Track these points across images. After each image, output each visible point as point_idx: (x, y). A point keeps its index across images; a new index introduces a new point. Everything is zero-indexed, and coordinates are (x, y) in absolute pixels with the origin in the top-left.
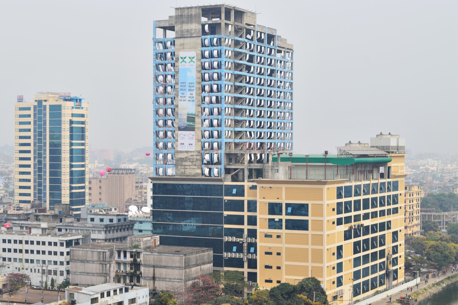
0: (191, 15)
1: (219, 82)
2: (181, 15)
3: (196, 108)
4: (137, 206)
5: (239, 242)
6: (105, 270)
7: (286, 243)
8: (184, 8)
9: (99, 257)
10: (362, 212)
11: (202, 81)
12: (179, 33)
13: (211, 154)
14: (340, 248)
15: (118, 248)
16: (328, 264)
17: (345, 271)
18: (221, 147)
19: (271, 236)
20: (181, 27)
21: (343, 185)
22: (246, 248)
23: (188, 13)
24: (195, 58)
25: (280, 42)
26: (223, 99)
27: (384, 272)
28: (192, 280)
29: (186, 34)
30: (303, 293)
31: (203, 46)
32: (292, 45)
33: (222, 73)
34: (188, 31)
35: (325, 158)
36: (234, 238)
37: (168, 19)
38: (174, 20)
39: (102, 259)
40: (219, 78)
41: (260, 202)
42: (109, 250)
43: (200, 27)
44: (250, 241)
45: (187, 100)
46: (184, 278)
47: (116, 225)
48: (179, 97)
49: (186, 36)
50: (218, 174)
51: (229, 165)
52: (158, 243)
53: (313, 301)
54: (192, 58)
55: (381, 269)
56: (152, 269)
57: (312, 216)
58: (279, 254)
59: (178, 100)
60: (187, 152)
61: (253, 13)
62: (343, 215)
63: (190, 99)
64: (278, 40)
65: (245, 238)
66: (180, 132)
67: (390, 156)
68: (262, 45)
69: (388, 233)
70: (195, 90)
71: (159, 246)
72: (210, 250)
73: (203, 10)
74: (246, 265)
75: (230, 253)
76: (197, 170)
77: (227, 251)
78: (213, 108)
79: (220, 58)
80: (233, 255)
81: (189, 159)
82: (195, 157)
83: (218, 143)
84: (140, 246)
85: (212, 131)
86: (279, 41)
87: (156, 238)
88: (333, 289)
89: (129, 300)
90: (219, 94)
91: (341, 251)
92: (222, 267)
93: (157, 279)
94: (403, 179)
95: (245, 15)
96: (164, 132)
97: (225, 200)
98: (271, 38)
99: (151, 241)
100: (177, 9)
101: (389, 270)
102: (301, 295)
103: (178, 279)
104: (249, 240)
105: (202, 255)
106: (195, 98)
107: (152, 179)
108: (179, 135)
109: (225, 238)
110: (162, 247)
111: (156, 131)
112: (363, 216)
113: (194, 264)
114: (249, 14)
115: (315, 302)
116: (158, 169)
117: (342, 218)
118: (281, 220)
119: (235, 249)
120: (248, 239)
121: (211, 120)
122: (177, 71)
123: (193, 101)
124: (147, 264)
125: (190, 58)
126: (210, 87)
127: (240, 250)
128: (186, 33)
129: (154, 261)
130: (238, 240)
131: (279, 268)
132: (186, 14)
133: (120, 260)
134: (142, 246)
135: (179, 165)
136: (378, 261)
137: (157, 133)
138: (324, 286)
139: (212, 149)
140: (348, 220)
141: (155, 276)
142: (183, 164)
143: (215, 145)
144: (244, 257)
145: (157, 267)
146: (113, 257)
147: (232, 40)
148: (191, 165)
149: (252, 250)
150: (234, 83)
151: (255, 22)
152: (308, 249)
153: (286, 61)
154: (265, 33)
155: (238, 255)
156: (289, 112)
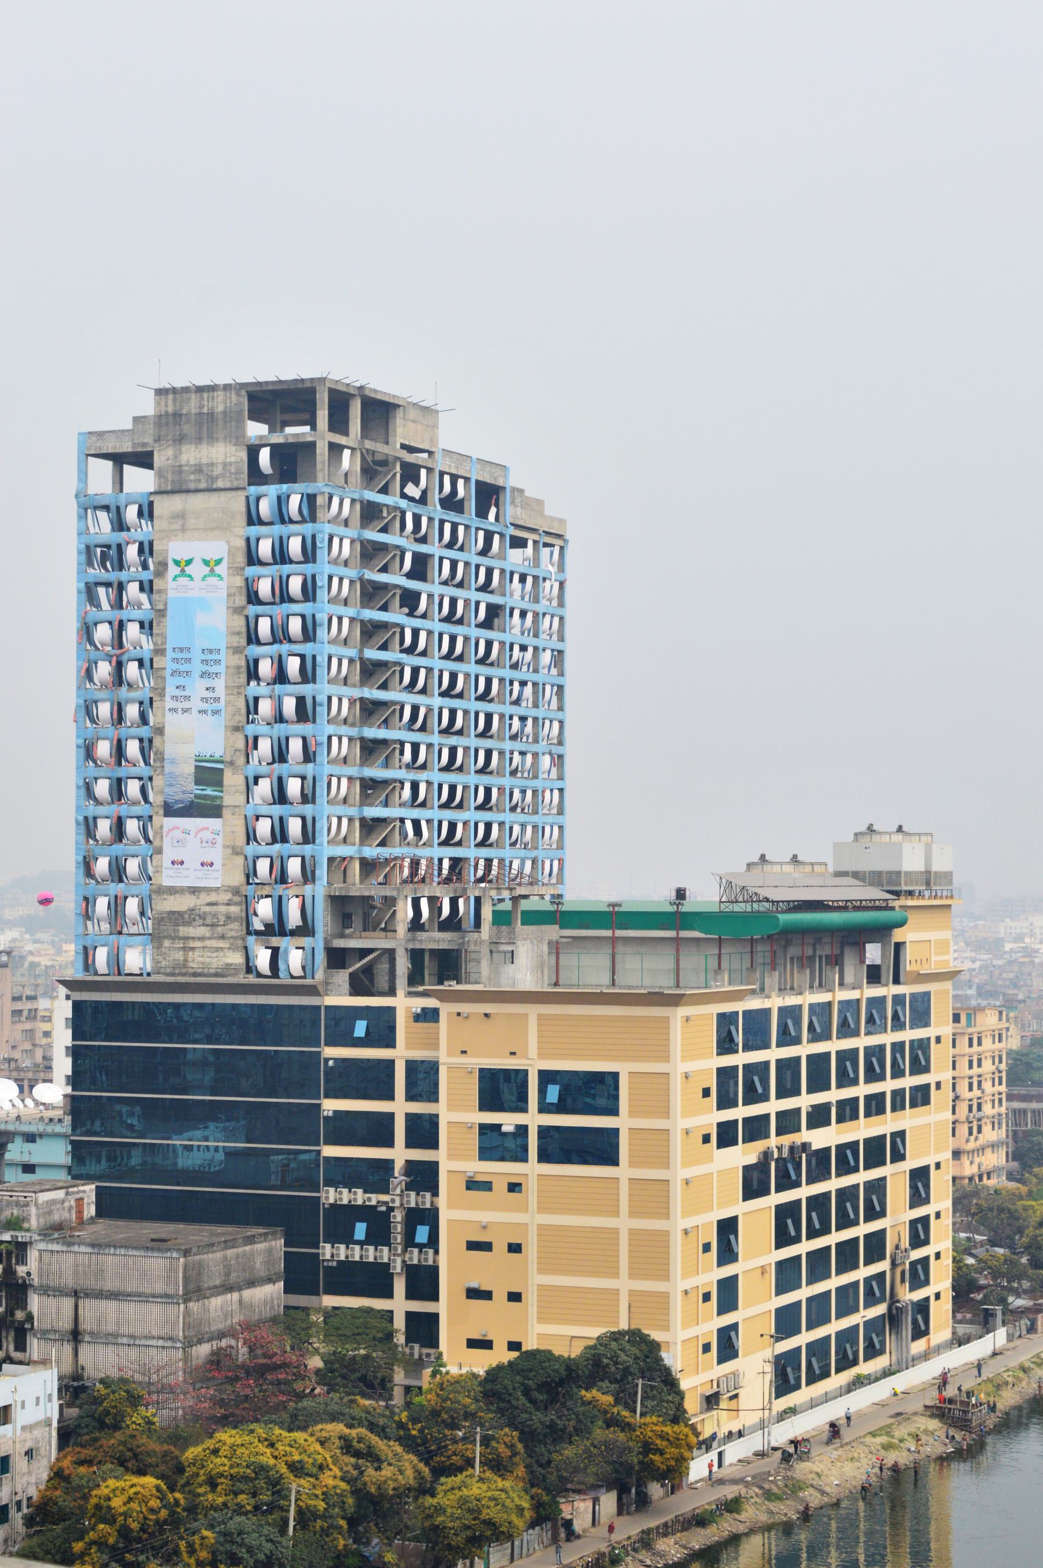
0: (211, 415)
1: (307, 649)
3: (226, 739)
4: (16, 1080)
5: (375, 1207)
7: (541, 1210)
8: (186, 390)
10: (805, 1101)
11: (249, 642)
12: (170, 477)
14: (728, 1227)
16: (688, 1284)
18: (313, 872)
19: (487, 1186)
20: (176, 457)
23: (201, 407)
24: (225, 564)
25: (519, 510)
27: (881, 1309)
28: (210, 1340)
30: (600, 1384)
31: (250, 522)
32: (562, 522)
33: (318, 616)
34: (199, 469)
36: (360, 1191)
37: (129, 425)
38: (151, 431)
43: (243, 455)
44: (413, 1205)
45: (195, 711)
46: (181, 1334)
48: (168, 698)
49: (192, 486)
50: (304, 968)
51: (342, 936)
52: (90, 1211)
53: (635, 1412)
54: (212, 563)
55: (872, 1300)
56: (68, 1303)
57: (632, 1114)
58: (515, 1248)
59: (164, 708)
60: (194, 891)
62: (740, 1113)
63: (205, 706)
64: (513, 502)
67: (901, 907)
68: (457, 520)
70: (223, 676)
74: (399, 1286)
75: (342, 1247)
78: (287, 739)
81: (203, 917)
82: (223, 909)
83: (303, 858)
84: (29, 1221)
85: (281, 818)
86: (516, 506)
87: (84, 1192)
90: (307, 690)
91: (732, 1237)
92: (317, 1294)
93: (87, 1338)
94: (948, 985)
97: (327, 1060)
99: (66, 1204)
100: (160, 392)
101: (898, 1301)
105: (244, 1253)
107: (72, 985)
109: (327, 1192)
112: (808, 1113)
113: (218, 1283)
114: (412, 413)
115: (642, 1415)
116: (91, 953)
118: (522, 1131)
119: (360, 1230)
120: (408, 1196)
121: (280, 779)
123: (216, 712)
124: (51, 1284)
125: (206, 563)
126: (276, 665)
127: (379, 1235)
128: (192, 477)
129: (76, 1273)
130: (374, 1199)
131: (515, 1297)
134: (34, 1223)
135: (165, 937)
136: (862, 1273)
138: (673, 1358)
139: (283, 878)
140: (756, 1128)
142: (181, 934)
143: (294, 867)
145: (87, 1295)
147: (353, 501)
148: (209, 938)
149: (422, 1234)
150: (361, 651)
151: (433, 440)
152: (616, 1231)
153: (541, 575)
154: (467, 480)
155: (371, 1254)
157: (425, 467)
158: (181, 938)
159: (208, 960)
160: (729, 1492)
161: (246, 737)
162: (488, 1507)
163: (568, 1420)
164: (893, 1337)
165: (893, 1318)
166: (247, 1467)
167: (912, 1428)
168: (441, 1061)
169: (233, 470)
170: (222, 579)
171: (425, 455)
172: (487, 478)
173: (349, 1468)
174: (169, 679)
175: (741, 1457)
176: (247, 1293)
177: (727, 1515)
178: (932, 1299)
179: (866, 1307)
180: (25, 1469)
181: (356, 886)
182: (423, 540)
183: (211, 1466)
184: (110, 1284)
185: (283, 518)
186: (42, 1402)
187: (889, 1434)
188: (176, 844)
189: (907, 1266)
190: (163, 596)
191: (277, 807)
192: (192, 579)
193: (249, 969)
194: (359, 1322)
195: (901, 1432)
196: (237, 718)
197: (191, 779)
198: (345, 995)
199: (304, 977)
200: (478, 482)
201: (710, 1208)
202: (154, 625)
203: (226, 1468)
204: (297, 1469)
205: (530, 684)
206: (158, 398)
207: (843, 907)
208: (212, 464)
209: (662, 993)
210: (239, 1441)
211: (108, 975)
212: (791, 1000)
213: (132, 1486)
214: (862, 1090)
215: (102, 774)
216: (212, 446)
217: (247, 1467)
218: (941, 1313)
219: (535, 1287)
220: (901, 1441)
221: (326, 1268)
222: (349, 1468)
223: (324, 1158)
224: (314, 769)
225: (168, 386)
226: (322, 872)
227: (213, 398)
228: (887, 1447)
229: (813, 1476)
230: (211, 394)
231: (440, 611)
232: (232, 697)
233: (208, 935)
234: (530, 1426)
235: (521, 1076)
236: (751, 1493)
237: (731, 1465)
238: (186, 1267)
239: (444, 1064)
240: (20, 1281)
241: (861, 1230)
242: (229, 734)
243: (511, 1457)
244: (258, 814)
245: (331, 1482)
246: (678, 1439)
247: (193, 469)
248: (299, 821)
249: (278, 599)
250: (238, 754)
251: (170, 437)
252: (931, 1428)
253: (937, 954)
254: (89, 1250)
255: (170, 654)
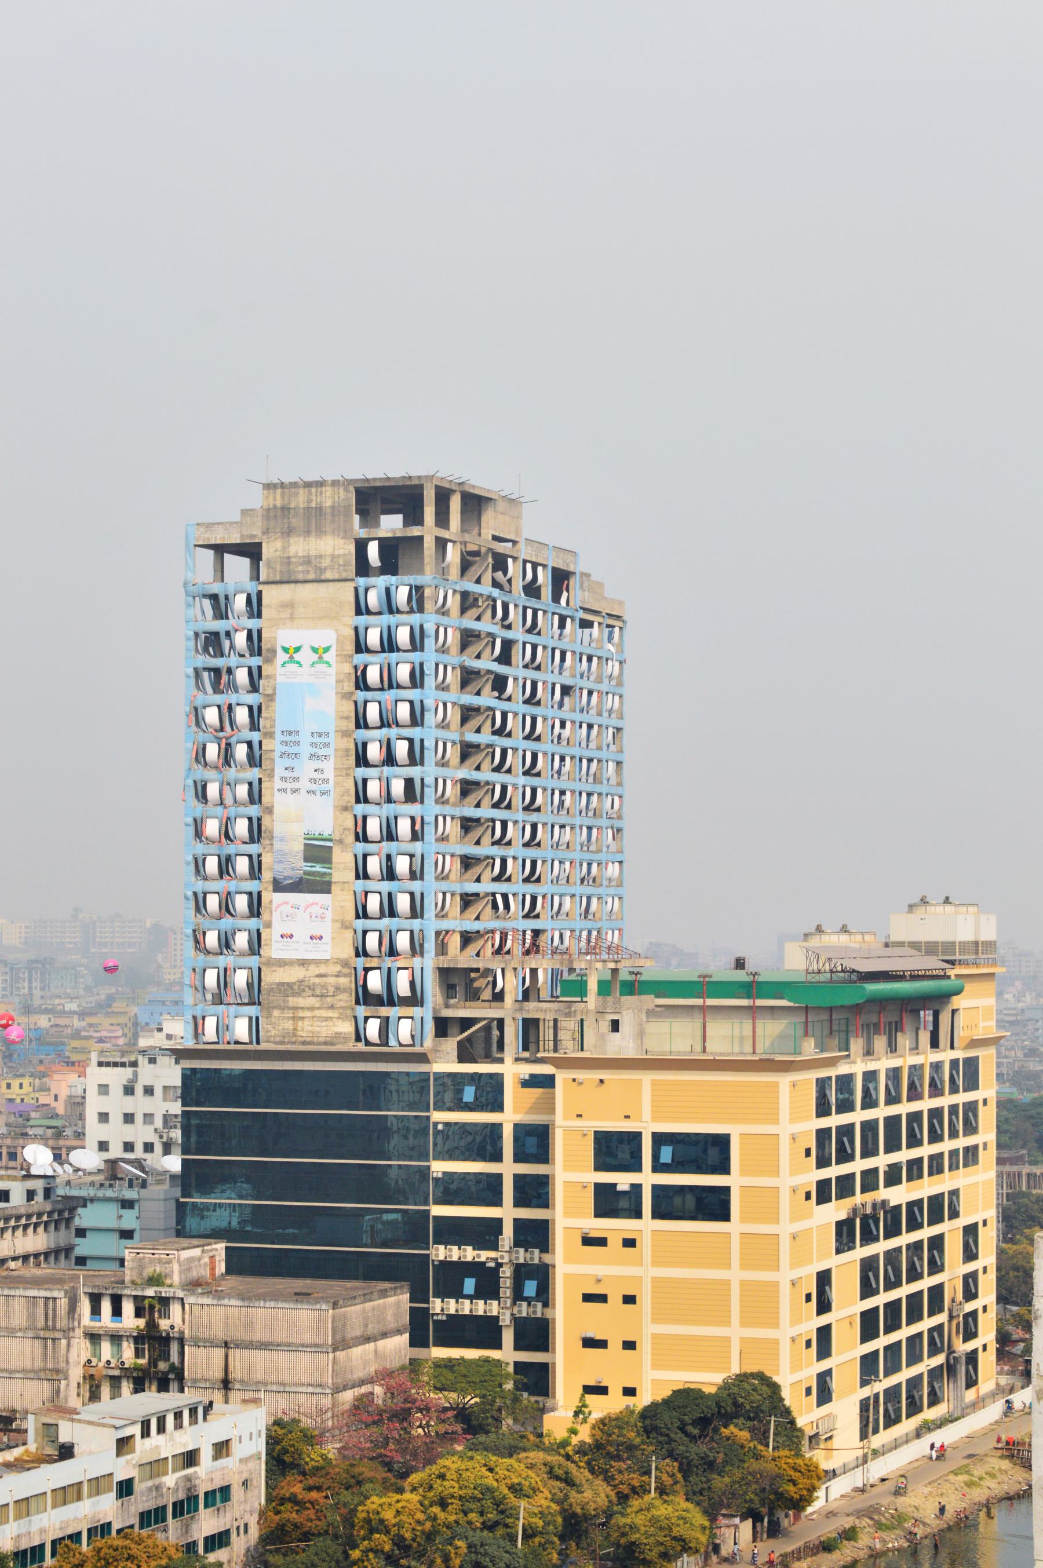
0: (320, 509)
1: (416, 733)
2: (283, 508)
3: (336, 818)
4: (53, 1148)
5: (484, 1263)
6: (54, 1357)
7: (655, 1263)
8: (294, 485)
9: (32, 1317)
10: (882, 1161)
11: (358, 726)
12: (278, 568)
13: (389, 969)
14: (824, 1279)
15: (94, 1287)
16: (794, 1331)
17: (837, 1355)
18: (422, 946)
19: (602, 1242)
20: (284, 548)
21: (832, 1072)
22: (508, 1283)
23: (310, 501)
24: (333, 652)
25: (586, 593)
26: (429, 786)
27: (940, 1359)
28: (353, 1387)
29: (300, 573)
30: (734, 1421)
31: (358, 612)
32: (621, 603)
33: (426, 702)
34: (307, 561)
35: (753, 982)
36: (469, 1249)
37: (237, 518)
38: (260, 524)
39: (41, 1323)
40: (416, 720)
41: (566, 1130)
42: (66, 1292)
43: (352, 548)
44: (521, 1261)
45: (303, 792)
46: (330, 1381)
47: (23, 1211)
48: (277, 779)
49: (301, 577)
50: (413, 1037)
51: (447, 1006)
52: (221, 1268)
53: (767, 1446)
54: (321, 651)
55: (934, 1351)
56: (218, 1353)
57: (744, 1172)
58: (629, 1300)
59: (273, 789)
60: (303, 963)
61: (513, 502)
62: (834, 1171)
63: (313, 787)
64: (581, 587)
65: (507, 1248)
66: (279, 897)
67: (957, 976)
68: (537, 606)
69: (951, 1230)
70: (332, 759)
71: (224, 1279)
72: (402, 1287)
73: (359, 492)
74: (508, 1337)
75: (452, 1301)
76: (339, 1023)
77: (443, 1293)
78: (396, 818)
79: (418, 654)
80: (466, 1307)
81: (312, 988)
82: (332, 980)
83: (412, 932)
84: (171, 1277)
85: (390, 894)
86: (584, 590)
87: (216, 1250)
88: (807, 1413)
89: (215, 1445)
90: (415, 772)
91: (827, 1288)
92: (428, 1346)
93: (237, 1386)
94: (992, 1051)
95: (491, 505)
96: (224, 897)
97: (436, 1124)
98: (561, 578)
99: (202, 1262)
100: (269, 486)
101: (954, 1352)
102: (732, 1427)
103: (309, 1385)
104: (522, 1256)
105: (379, 1305)
106: (331, 782)
107: (179, 1054)
108: (277, 908)
109: (437, 1249)
110: (233, 1281)
111: (195, 894)
112: (885, 1172)
113: (358, 1333)
114: (501, 506)
115: (774, 1449)
116: (200, 1022)
117: (830, 1179)
118: (637, 1188)
119: (469, 1285)
120: (517, 1252)
121: (389, 857)
122: (270, 692)
123: (324, 793)
124: (202, 1336)
125: (315, 650)
126: (384, 748)
127: (488, 1288)
128: (300, 568)
129: (226, 1324)
130: (484, 1255)
131: (629, 1345)
132: (301, 506)
133: (98, 1324)
134: (176, 1279)
135: (275, 1007)
136: (926, 1324)
137: (200, 903)
138: (788, 1396)
139: (393, 952)
140: (845, 1186)
141: (231, 1376)
142: (290, 1004)
143: (403, 941)
144: (504, 1314)
145: (237, 1346)
146: (76, 1316)
147: (455, 591)
148: (319, 1008)
149: (530, 1288)
150: (462, 734)
151: (518, 531)
152: (727, 1283)
153: (605, 656)
154: (544, 566)
155: (480, 1308)
156: (612, 828)
157: (511, 557)
158: (290, 1008)
159: (318, 1029)
160: (847, 1523)
161: (355, 816)
162: (678, 1525)
163: (718, 1452)
164: (951, 1385)
165: (950, 1368)
166: (475, 1488)
167: (988, 1468)
168: (557, 1124)
169: (341, 562)
170: (330, 666)
171: (510, 544)
172: (561, 565)
173: (556, 1491)
174: (278, 760)
175: (843, 1492)
176: (381, 1343)
177: (845, 1542)
178: (980, 1350)
179: (929, 1357)
180: (242, 1498)
181: (460, 958)
182: (509, 627)
183: (440, 1489)
184: (259, 1335)
185: (391, 609)
186: (254, 1437)
187: (968, 1472)
188: (285, 918)
189: (961, 1319)
190: (272, 681)
191: (386, 883)
192: (301, 666)
193: (359, 1036)
194: (483, 1370)
195: (978, 1471)
196: (346, 798)
197: (300, 856)
198: (453, 1062)
199: (413, 1045)
200: (554, 569)
201: (810, 1261)
202: (263, 708)
203: (456, 1490)
204: (516, 1491)
205: (595, 761)
206: (266, 492)
207: (915, 977)
208: (321, 557)
209: (773, 1060)
210: (463, 1467)
211: (217, 1043)
212: (871, 1066)
213: (398, 1501)
214: (925, 1151)
215: (212, 852)
216: (321, 539)
217: (475, 1488)
218: (987, 1361)
219: (649, 1336)
220: (981, 1479)
221: (435, 1322)
222: (556, 1491)
223: (434, 1217)
224: (423, 848)
225: (276, 481)
226: (430, 946)
227: (321, 493)
228: (970, 1484)
229: (912, 1509)
230: (319, 489)
231: (524, 693)
232: (340, 778)
233: (317, 1005)
234: (686, 1458)
235: (635, 1138)
236: (864, 1523)
237: (836, 1500)
238: (334, 1317)
239: (560, 1127)
240: (164, 1334)
241: (925, 1284)
242: (338, 813)
243: (672, 1485)
244: (367, 889)
245: (545, 1503)
246: (809, 1471)
247: (301, 560)
248: (407, 897)
249: (386, 685)
250: (347, 832)
251: (278, 530)
252: (1003, 1468)
253: (984, 1020)
254: (239, 1303)
255: (279, 737)
